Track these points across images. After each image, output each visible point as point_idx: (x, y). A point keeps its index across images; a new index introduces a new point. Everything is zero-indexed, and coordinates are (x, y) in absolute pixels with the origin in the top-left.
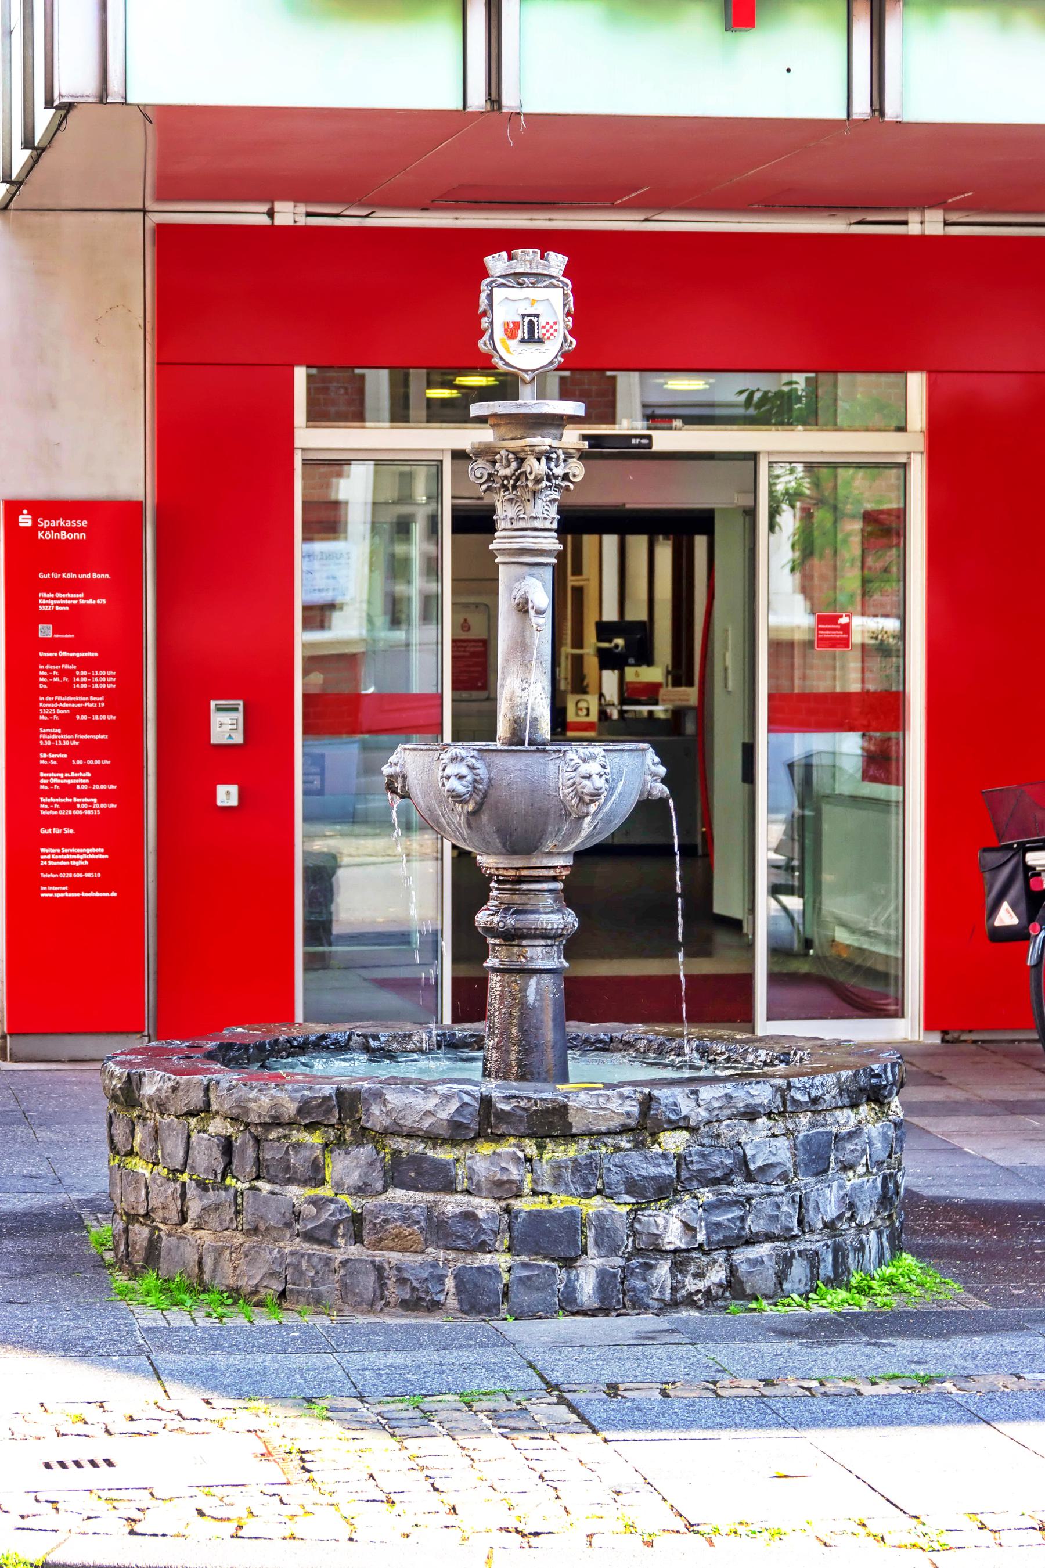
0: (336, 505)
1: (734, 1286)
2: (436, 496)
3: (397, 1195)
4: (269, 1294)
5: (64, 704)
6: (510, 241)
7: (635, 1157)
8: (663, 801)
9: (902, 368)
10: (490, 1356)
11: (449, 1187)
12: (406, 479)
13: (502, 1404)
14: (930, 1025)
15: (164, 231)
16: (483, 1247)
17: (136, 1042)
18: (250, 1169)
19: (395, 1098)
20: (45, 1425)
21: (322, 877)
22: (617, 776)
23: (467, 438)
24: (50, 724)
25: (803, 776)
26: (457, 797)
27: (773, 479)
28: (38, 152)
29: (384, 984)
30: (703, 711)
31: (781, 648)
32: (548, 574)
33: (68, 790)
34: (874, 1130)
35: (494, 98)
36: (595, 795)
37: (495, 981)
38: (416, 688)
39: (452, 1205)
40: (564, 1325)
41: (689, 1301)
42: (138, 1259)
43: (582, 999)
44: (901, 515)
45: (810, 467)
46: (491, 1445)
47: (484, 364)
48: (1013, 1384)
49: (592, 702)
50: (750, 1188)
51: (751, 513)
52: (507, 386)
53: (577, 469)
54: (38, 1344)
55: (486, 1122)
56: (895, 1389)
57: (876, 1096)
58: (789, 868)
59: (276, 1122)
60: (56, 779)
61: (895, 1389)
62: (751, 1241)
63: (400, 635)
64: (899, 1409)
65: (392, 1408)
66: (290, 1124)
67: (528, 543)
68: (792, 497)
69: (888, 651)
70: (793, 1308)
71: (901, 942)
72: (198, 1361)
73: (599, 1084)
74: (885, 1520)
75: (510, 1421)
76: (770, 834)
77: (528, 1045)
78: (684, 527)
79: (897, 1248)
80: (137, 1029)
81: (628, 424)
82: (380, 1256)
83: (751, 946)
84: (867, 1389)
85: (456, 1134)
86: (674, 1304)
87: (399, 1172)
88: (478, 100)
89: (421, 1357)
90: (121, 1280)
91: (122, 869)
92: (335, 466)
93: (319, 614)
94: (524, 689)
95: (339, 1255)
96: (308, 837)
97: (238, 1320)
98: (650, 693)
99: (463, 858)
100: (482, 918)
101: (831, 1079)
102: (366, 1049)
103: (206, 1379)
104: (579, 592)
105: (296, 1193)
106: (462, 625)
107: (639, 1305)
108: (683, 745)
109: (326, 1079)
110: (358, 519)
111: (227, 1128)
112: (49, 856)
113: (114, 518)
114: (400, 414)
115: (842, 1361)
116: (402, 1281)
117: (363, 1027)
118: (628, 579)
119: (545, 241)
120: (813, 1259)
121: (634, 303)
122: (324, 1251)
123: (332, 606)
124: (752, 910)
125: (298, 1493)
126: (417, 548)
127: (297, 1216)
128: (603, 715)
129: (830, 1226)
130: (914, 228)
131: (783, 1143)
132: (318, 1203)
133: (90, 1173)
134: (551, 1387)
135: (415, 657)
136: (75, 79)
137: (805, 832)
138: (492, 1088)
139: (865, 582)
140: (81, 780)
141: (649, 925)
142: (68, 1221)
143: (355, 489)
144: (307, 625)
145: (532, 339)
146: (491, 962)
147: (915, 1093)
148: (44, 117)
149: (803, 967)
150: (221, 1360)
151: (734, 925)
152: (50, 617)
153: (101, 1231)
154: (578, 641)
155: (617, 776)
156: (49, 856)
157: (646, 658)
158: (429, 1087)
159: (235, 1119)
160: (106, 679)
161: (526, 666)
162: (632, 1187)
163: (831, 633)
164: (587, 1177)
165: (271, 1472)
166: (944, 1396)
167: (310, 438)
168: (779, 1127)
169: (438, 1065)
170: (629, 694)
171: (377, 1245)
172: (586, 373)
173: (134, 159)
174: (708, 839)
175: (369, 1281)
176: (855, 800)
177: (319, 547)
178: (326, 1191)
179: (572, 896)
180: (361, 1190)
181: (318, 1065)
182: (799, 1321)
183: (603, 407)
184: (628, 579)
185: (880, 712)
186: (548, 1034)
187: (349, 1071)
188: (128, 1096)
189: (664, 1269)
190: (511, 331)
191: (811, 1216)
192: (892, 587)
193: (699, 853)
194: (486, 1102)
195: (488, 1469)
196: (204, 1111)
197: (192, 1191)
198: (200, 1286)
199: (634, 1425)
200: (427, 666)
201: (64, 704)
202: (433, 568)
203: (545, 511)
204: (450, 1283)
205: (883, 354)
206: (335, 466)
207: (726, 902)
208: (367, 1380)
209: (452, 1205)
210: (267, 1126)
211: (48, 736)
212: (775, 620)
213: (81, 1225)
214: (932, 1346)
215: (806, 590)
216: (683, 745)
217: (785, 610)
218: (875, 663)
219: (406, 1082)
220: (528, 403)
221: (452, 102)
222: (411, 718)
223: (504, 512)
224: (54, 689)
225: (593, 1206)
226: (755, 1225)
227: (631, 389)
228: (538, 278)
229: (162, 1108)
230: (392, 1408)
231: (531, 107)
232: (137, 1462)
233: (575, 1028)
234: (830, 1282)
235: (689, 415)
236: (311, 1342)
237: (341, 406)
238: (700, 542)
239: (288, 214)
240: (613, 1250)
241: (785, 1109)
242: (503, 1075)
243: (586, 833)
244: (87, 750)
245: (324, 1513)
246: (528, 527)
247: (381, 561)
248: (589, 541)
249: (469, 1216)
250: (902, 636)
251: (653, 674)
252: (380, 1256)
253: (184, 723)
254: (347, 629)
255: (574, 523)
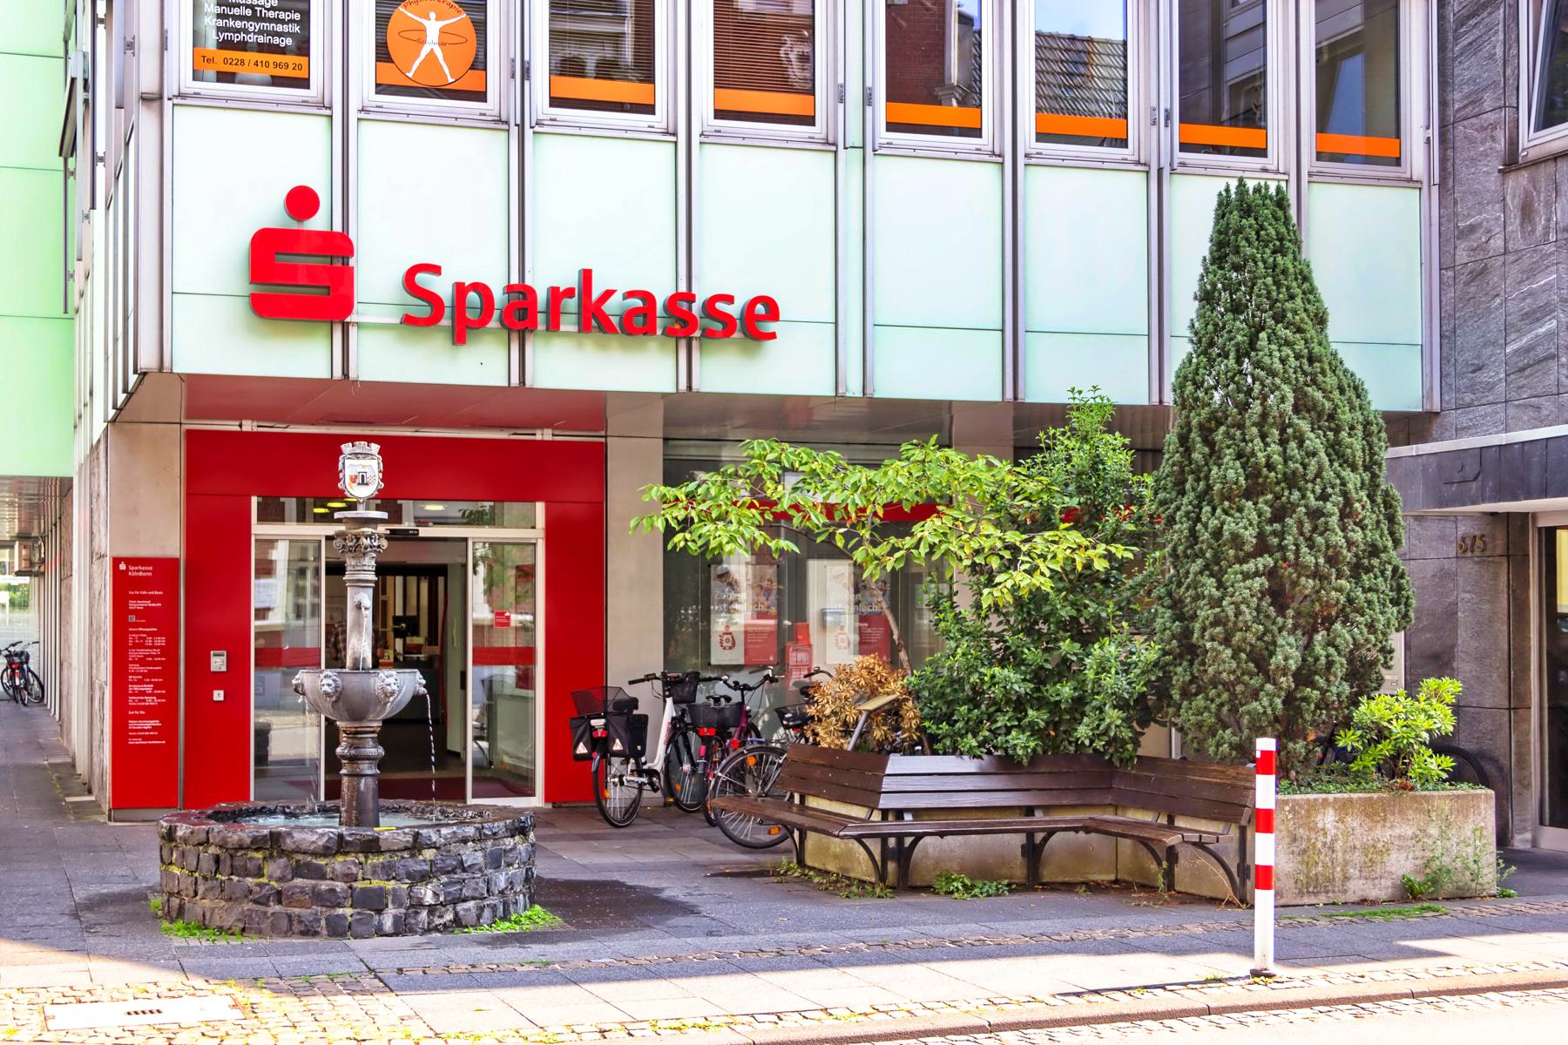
0: (271, 562)
1: (458, 922)
2: (318, 558)
3: (298, 881)
4: (237, 930)
5: (141, 652)
6: (352, 439)
7: (411, 862)
8: (424, 696)
9: (534, 500)
10: (342, 957)
11: (323, 877)
12: (304, 550)
13: (348, 979)
14: (547, 800)
15: (190, 433)
16: (339, 905)
17: (173, 811)
18: (228, 870)
19: (297, 835)
20: (129, 994)
21: (263, 735)
22: (402, 684)
23: (331, 529)
24: (134, 662)
25: (489, 685)
26: (327, 694)
27: (475, 550)
28: (130, 395)
29: (293, 783)
30: (442, 658)
31: (479, 628)
32: (371, 591)
33: (143, 693)
34: (522, 847)
35: (346, 374)
36: (392, 693)
37: (345, 780)
38: (309, 645)
39: (324, 886)
40: (378, 941)
41: (436, 929)
42: (174, 914)
43: (386, 789)
44: (533, 567)
45: (491, 544)
46: (343, 999)
47: (341, 495)
48: (587, 965)
49: (390, 653)
50: (464, 875)
51: (465, 566)
52: (352, 506)
53: (385, 543)
54: (124, 957)
55: (340, 846)
56: (532, 968)
57: (523, 831)
58: (482, 728)
59: (241, 848)
60: (137, 688)
61: (532, 968)
62: (465, 900)
63: (301, 622)
64: (534, 977)
65: (295, 982)
66: (248, 848)
67: (362, 577)
68: (483, 558)
69: (528, 629)
70: (485, 931)
71: (534, 762)
72: (203, 962)
73: (392, 827)
74: (528, 1030)
75: (353, 987)
76: (473, 713)
77: (361, 809)
78: (433, 573)
79: (532, 903)
80: (174, 806)
81: (407, 524)
82: (291, 910)
83: (464, 764)
84: (519, 969)
85: (326, 852)
86: (429, 931)
87: (299, 870)
88: (338, 374)
89: (309, 957)
90: (166, 924)
91: (168, 730)
92: (270, 543)
93: (262, 613)
94: (360, 644)
95: (270, 910)
96: (257, 716)
97: (222, 942)
98: (418, 649)
99: (330, 724)
100: (339, 750)
101: (502, 824)
102: (284, 813)
103: (209, 974)
104: (385, 603)
105: (249, 880)
106: (330, 617)
107: (412, 931)
108: (435, 671)
109: (265, 827)
110: (281, 568)
111: (218, 851)
112: (132, 724)
113: (164, 566)
114: (301, 518)
115: (509, 955)
116: (300, 922)
117: (282, 803)
118: (407, 596)
119: (370, 439)
120: (494, 908)
121: (408, 469)
122: (263, 908)
123: (269, 609)
124: (465, 748)
125: (251, 1023)
126: (309, 582)
127: (251, 892)
128: (396, 659)
129: (502, 892)
130: (538, 437)
131: (479, 854)
132: (260, 885)
133: (151, 873)
134: (371, 970)
135: (308, 632)
136: (148, 360)
137: (489, 711)
138: (343, 830)
139: (517, 597)
140: (148, 688)
141: (416, 754)
142: (140, 897)
143: (280, 555)
144: (257, 618)
145: (363, 483)
146: (343, 771)
147: (542, 831)
148: (133, 378)
149: (489, 774)
150: (214, 961)
151: (457, 755)
152: (135, 612)
153: (156, 901)
154: (384, 625)
155: (402, 684)
156: (132, 724)
157: (416, 633)
158: (315, 829)
159: (221, 847)
160: (161, 641)
161: (360, 633)
162: (409, 875)
163: (502, 620)
164: (388, 871)
165: (237, 1014)
166: (555, 971)
167: (259, 529)
168: (478, 846)
169: (319, 820)
170: (408, 649)
171: (289, 905)
172: (387, 500)
173: (175, 403)
174: (445, 716)
175: (284, 923)
176: (513, 697)
177: (263, 581)
178: (264, 880)
179: (381, 740)
180: (281, 879)
181: (261, 821)
182: (488, 937)
183: (396, 516)
184: (407, 596)
185: (523, 657)
186: (370, 804)
187: (277, 823)
188: (170, 836)
189: (424, 914)
190: (353, 480)
191: (493, 888)
192: (529, 600)
193: (441, 722)
194: (341, 836)
195: (344, 1011)
196: (206, 843)
197: (200, 881)
198: (203, 926)
199: (411, 989)
200: (314, 635)
201: (141, 652)
202: (316, 591)
203: (370, 562)
204: (323, 922)
205: (527, 495)
206: (270, 543)
207: (453, 744)
208: (283, 969)
209: (324, 886)
210: (236, 850)
211: (133, 667)
212: (475, 616)
213: (146, 898)
214: (549, 948)
215: (490, 602)
216: (435, 671)
217: (479, 610)
218: (522, 634)
219: (303, 828)
220: (361, 512)
221: (326, 375)
222: (307, 659)
223: (350, 562)
224: (136, 646)
225: (391, 885)
226: (466, 892)
227: (408, 506)
228: (366, 455)
229: (186, 841)
230: (295, 982)
231: (364, 377)
232: (173, 1012)
233: (383, 802)
234: (502, 919)
235: (435, 519)
236: (257, 952)
237: (272, 513)
238: (441, 580)
239: (248, 426)
240: (400, 906)
241: (481, 838)
242: (348, 824)
243: (389, 711)
244: (151, 674)
245: (263, 1033)
246: (364, 569)
247: (292, 587)
248: (389, 579)
249: (332, 891)
250: (534, 622)
251: (419, 640)
252: (291, 910)
253: (198, 661)
254: (276, 619)
255: (383, 570)
